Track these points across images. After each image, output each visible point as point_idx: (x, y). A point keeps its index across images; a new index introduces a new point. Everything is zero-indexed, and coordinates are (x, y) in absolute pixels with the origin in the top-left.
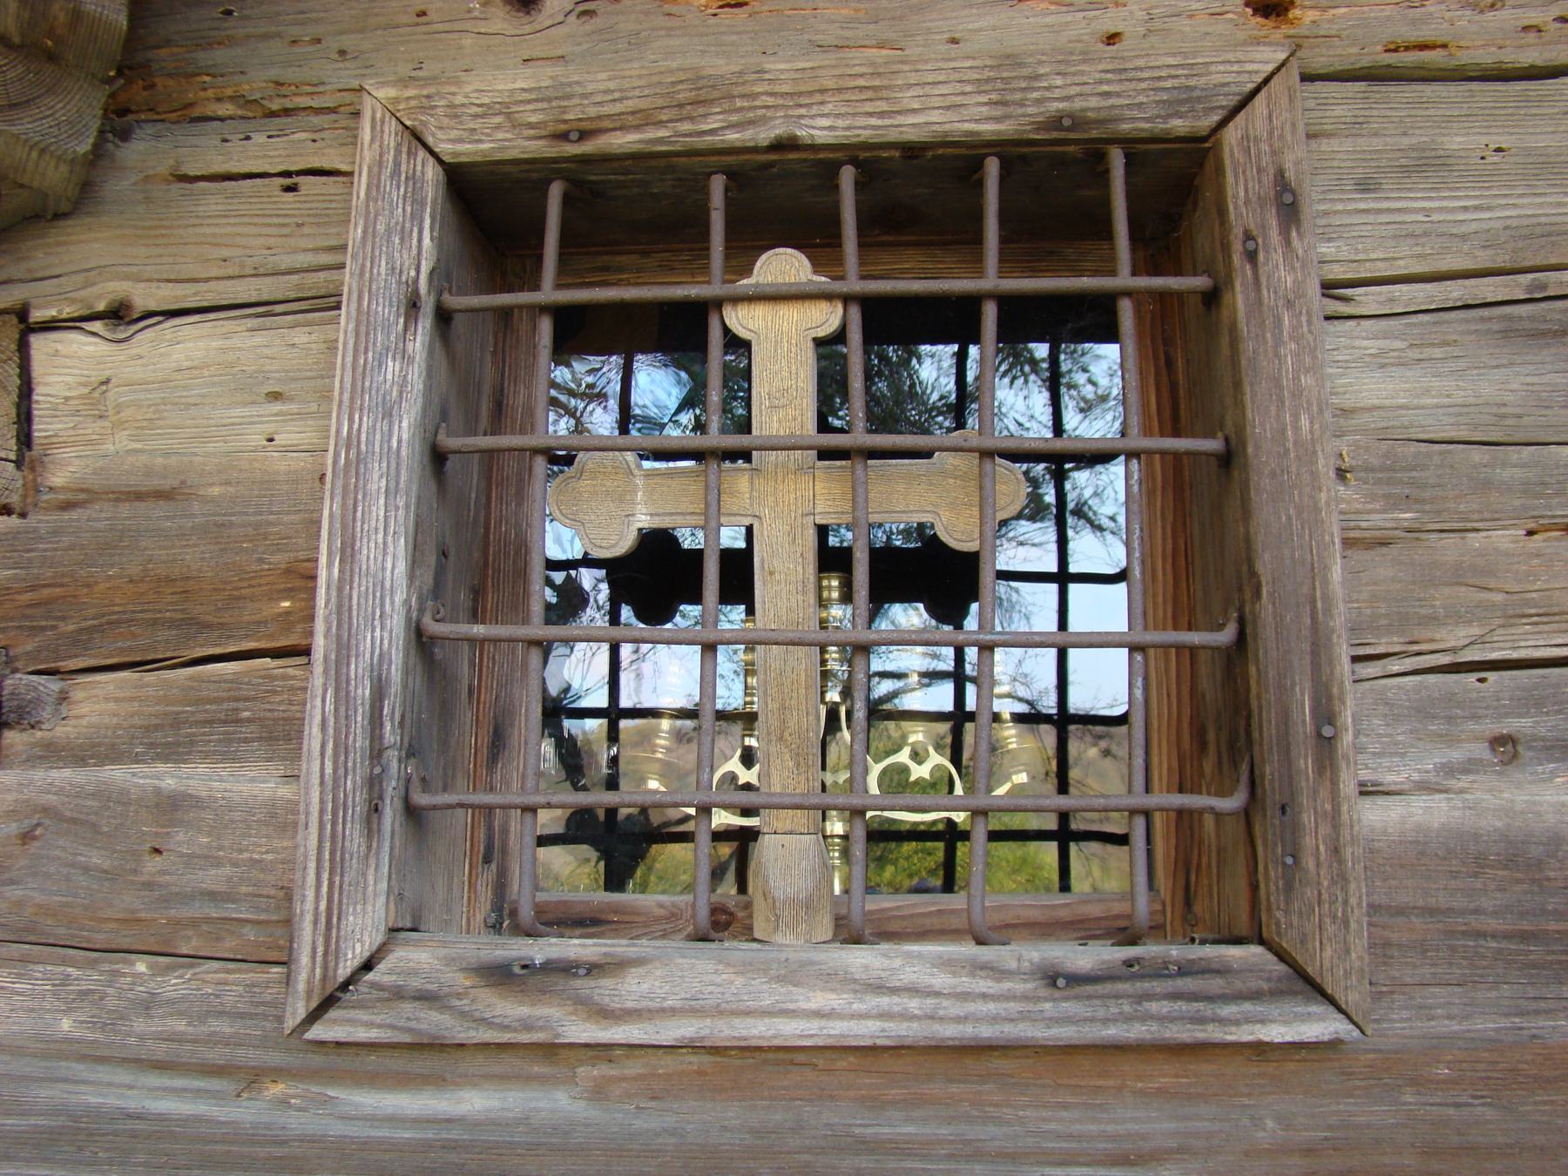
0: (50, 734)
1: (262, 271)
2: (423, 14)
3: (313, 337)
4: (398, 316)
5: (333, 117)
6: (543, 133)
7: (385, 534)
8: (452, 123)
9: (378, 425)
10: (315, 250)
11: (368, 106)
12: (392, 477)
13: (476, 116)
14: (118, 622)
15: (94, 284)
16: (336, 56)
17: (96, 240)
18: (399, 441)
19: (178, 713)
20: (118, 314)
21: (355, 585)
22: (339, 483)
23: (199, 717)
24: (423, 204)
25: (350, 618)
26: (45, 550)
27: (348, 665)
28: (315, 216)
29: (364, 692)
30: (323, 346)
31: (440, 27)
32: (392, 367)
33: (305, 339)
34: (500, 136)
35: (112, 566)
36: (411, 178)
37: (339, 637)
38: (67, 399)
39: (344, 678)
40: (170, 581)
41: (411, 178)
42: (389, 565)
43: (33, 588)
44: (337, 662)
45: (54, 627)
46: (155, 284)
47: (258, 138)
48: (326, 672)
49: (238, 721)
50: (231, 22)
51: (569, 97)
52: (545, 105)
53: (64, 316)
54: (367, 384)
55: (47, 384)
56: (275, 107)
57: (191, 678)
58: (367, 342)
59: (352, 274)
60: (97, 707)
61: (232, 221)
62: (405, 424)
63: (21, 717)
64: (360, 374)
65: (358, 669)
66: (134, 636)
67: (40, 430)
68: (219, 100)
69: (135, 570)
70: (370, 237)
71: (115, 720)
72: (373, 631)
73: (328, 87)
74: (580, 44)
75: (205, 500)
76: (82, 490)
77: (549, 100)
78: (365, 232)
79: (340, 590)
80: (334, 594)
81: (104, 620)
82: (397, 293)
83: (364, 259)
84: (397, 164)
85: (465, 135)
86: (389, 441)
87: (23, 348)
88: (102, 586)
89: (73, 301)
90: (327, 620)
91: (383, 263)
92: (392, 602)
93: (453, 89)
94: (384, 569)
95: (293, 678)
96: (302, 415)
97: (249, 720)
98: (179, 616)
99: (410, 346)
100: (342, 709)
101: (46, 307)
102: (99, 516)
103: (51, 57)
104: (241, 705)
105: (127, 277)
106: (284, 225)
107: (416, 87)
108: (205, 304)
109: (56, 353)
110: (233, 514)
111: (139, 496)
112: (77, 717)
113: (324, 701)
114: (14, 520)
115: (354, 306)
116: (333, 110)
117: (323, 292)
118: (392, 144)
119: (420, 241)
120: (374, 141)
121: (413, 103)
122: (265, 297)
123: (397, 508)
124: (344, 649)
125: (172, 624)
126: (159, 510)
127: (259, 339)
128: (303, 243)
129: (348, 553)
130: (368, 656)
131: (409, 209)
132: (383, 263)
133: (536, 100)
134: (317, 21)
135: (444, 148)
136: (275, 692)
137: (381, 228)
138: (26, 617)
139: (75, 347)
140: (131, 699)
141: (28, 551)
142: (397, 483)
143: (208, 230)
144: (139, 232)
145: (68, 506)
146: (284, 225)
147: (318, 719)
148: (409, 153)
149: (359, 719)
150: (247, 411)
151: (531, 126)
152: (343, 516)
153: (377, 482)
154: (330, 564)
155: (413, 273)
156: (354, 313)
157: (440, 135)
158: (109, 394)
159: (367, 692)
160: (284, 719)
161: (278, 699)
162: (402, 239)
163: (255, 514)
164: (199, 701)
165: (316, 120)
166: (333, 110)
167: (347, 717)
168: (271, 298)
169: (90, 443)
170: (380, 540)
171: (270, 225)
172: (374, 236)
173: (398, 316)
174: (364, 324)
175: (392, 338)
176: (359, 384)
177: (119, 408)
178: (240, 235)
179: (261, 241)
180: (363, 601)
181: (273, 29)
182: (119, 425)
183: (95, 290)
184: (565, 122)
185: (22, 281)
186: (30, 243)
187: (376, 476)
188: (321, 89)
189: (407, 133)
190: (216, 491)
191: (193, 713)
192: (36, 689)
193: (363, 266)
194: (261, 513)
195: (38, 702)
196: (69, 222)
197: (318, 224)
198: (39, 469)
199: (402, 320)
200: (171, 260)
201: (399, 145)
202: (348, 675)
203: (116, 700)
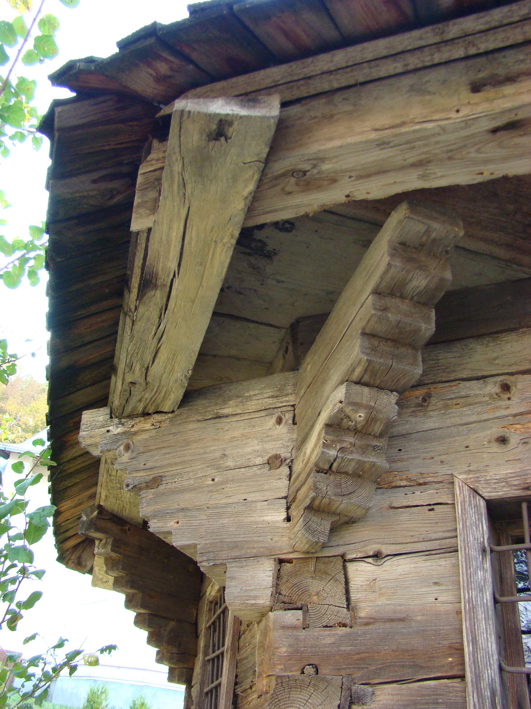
0: (369, 707)
1: (426, 539)
2: (467, 447)
3: (447, 562)
4: (479, 555)
5: (442, 484)
6: (520, 488)
7: (487, 634)
8: (487, 486)
9: (478, 595)
10: (443, 532)
11: (456, 481)
12: (486, 612)
13: (495, 483)
14: (390, 666)
15: (367, 546)
16: (439, 463)
17: (366, 530)
18: (487, 600)
19: (415, 700)
20: (377, 556)
21: (479, 653)
22: (468, 616)
23: (423, 701)
24: (481, 515)
25: (479, 666)
26: (361, 640)
27: (481, 684)
28: (442, 519)
29: (488, 693)
30: (451, 565)
31: (474, 451)
32: (480, 573)
33: (444, 563)
34: (505, 489)
35: (386, 645)
36: (476, 506)
37: (475, 673)
38: (362, 585)
39: (479, 688)
40: (407, 651)
41: (476, 506)
42: (490, 646)
43: (358, 654)
44: (476, 682)
45: (367, 668)
46: (388, 545)
47: (418, 493)
48: (472, 686)
49: (438, 703)
50: (401, 453)
51: (527, 475)
52: (519, 478)
53: (358, 557)
54: (472, 580)
55: (355, 581)
56: (421, 481)
57: (419, 687)
58: (470, 565)
59: (461, 541)
60: (385, 697)
61: (412, 522)
62: (488, 594)
63: (359, 701)
64: (469, 576)
65: (484, 684)
66: (396, 671)
67: (353, 596)
68: (401, 480)
69: (394, 647)
70: (465, 527)
71: (392, 702)
72: (488, 670)
73: (439, 474)
74: (525, 455)
75: (416, 621)
76: (371, 618)
77: (520, 476)
78: (463, 525)
79: (473, 655)
80: (471, 656)
81: (385, 665)
82: (477, 547)
83: (464, 535)
84: (470, 501)
85: (492, 490)
86: (483, 600)
87: (345, 568)
88: (383, 653)
89: (361, 552)
90: (470, 666)
91: (471, 537)
92: (493, 660)
93: (486, 474)
94: (488, 647)
95: (456, 687)
96: (447, 590)
97: (442, 703)
98: (412, 664)
99: (485, 565)
100: (481, 700)
101: (351, 554)
102: (379, 627)
103: (360, 476)
104: (438, 697)
105: (378, 543)
106: (431, 523)
107: (473, 474)
108: (408, 552)
109: (357, 570)
110: (426, 627)
111: (392, 620)
112: (378, 701)
113: (473, 697)
114: (348, 629)
115: (463, 552)
116: (441, 482)
117: (448, 546)
118: (467, 494)
119: (483, 528)
120: (461, 494)
121: (472, 480)
122: (428, 549)
123: (490, 625)
124: (478, 677)
125: (411, 667)
126: (401, 625)
127: (428, 564)
128: (439, 529)
129: (474, 641)
130: (487, 680)
131: (477, 517)
132: (471, 537)
133: (516, 476)
134: (432, 451)
135: (486, 495)
136: (450, 692)
137: (468, 524)
138: (357, 664)
139: (363, 568)
140: (397, 695)
141: (356, 640)
142: (488, 615)
143: (405, 526)
144: (380, 527)
145: (367, 624)
146: (431, 523)
147: (472, 704)
148: (473, 497)
149: (487, 704)
150: (427, 589)
151: (515, 485)
152: (471, 628)
153: (481, 615)
154: (468, 646)
155: (482, 540)
156: (464, 555)
157: (484, 490)
158: (376, 584)
159: (489, 694)
160: (455, 703)
161: (452, 695)
162: (476, 528)
163: (434, 626)
164: (423, 695)
165: (437, 486)
166: (441, 482)
167: (483, 703)
168: (430, 549)
169: (372, 601)
170: (485, 636)
171: (426, 523)
172: (466, 527)
173: (479, 555)
174: (467, 557)
175: (479, 563)
176: (469, 580)
177: (380, 589)
178: (415, 526)
179: (424, 529)
180: (482, 659)
181: (417, 455)
182: (381, 595)
183: (368, 548)
184: (527, 483)
185: (342, 545)
186: (343, 532)
187: (480, 613)
188: (437, 475)
189: (471, 490)
190: (419, 618)
191: (421, 700)
192: (364, 691)
193: (464, 538)
194: (437, 626)
195: (365, 695)
196: (356, 524)
197: (443, 522)
198: (355, 611)
199: (481, 556)
200: (393, 536)
201: (469, 494)
202: (481, 687)
203: (392, 695)
